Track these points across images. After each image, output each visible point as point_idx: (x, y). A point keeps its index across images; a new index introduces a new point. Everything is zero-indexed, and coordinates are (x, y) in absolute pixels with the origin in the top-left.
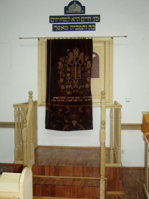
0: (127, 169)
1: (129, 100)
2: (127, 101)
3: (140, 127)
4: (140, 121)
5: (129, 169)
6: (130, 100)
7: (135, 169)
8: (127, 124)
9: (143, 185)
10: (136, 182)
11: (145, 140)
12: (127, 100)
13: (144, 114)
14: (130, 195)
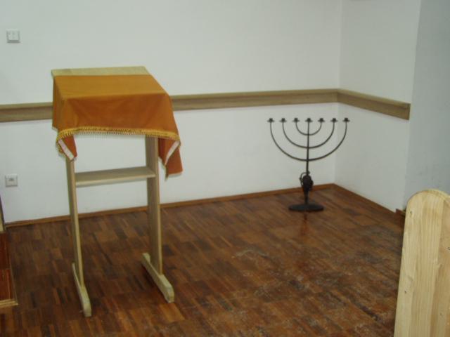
0: (29, 226)
1: (16, 38)
2: (10, 42)
3: (50, 113)
4: (45, 96)
5: (34, 225)
6: (19, 38)
7: (50, 223)
8: (16, 105)
9: (71, 265)
10: (54, 262)
11: (61, 151)
12: (10, 39)
13: (55, 74)
14: (34, 305)
